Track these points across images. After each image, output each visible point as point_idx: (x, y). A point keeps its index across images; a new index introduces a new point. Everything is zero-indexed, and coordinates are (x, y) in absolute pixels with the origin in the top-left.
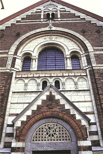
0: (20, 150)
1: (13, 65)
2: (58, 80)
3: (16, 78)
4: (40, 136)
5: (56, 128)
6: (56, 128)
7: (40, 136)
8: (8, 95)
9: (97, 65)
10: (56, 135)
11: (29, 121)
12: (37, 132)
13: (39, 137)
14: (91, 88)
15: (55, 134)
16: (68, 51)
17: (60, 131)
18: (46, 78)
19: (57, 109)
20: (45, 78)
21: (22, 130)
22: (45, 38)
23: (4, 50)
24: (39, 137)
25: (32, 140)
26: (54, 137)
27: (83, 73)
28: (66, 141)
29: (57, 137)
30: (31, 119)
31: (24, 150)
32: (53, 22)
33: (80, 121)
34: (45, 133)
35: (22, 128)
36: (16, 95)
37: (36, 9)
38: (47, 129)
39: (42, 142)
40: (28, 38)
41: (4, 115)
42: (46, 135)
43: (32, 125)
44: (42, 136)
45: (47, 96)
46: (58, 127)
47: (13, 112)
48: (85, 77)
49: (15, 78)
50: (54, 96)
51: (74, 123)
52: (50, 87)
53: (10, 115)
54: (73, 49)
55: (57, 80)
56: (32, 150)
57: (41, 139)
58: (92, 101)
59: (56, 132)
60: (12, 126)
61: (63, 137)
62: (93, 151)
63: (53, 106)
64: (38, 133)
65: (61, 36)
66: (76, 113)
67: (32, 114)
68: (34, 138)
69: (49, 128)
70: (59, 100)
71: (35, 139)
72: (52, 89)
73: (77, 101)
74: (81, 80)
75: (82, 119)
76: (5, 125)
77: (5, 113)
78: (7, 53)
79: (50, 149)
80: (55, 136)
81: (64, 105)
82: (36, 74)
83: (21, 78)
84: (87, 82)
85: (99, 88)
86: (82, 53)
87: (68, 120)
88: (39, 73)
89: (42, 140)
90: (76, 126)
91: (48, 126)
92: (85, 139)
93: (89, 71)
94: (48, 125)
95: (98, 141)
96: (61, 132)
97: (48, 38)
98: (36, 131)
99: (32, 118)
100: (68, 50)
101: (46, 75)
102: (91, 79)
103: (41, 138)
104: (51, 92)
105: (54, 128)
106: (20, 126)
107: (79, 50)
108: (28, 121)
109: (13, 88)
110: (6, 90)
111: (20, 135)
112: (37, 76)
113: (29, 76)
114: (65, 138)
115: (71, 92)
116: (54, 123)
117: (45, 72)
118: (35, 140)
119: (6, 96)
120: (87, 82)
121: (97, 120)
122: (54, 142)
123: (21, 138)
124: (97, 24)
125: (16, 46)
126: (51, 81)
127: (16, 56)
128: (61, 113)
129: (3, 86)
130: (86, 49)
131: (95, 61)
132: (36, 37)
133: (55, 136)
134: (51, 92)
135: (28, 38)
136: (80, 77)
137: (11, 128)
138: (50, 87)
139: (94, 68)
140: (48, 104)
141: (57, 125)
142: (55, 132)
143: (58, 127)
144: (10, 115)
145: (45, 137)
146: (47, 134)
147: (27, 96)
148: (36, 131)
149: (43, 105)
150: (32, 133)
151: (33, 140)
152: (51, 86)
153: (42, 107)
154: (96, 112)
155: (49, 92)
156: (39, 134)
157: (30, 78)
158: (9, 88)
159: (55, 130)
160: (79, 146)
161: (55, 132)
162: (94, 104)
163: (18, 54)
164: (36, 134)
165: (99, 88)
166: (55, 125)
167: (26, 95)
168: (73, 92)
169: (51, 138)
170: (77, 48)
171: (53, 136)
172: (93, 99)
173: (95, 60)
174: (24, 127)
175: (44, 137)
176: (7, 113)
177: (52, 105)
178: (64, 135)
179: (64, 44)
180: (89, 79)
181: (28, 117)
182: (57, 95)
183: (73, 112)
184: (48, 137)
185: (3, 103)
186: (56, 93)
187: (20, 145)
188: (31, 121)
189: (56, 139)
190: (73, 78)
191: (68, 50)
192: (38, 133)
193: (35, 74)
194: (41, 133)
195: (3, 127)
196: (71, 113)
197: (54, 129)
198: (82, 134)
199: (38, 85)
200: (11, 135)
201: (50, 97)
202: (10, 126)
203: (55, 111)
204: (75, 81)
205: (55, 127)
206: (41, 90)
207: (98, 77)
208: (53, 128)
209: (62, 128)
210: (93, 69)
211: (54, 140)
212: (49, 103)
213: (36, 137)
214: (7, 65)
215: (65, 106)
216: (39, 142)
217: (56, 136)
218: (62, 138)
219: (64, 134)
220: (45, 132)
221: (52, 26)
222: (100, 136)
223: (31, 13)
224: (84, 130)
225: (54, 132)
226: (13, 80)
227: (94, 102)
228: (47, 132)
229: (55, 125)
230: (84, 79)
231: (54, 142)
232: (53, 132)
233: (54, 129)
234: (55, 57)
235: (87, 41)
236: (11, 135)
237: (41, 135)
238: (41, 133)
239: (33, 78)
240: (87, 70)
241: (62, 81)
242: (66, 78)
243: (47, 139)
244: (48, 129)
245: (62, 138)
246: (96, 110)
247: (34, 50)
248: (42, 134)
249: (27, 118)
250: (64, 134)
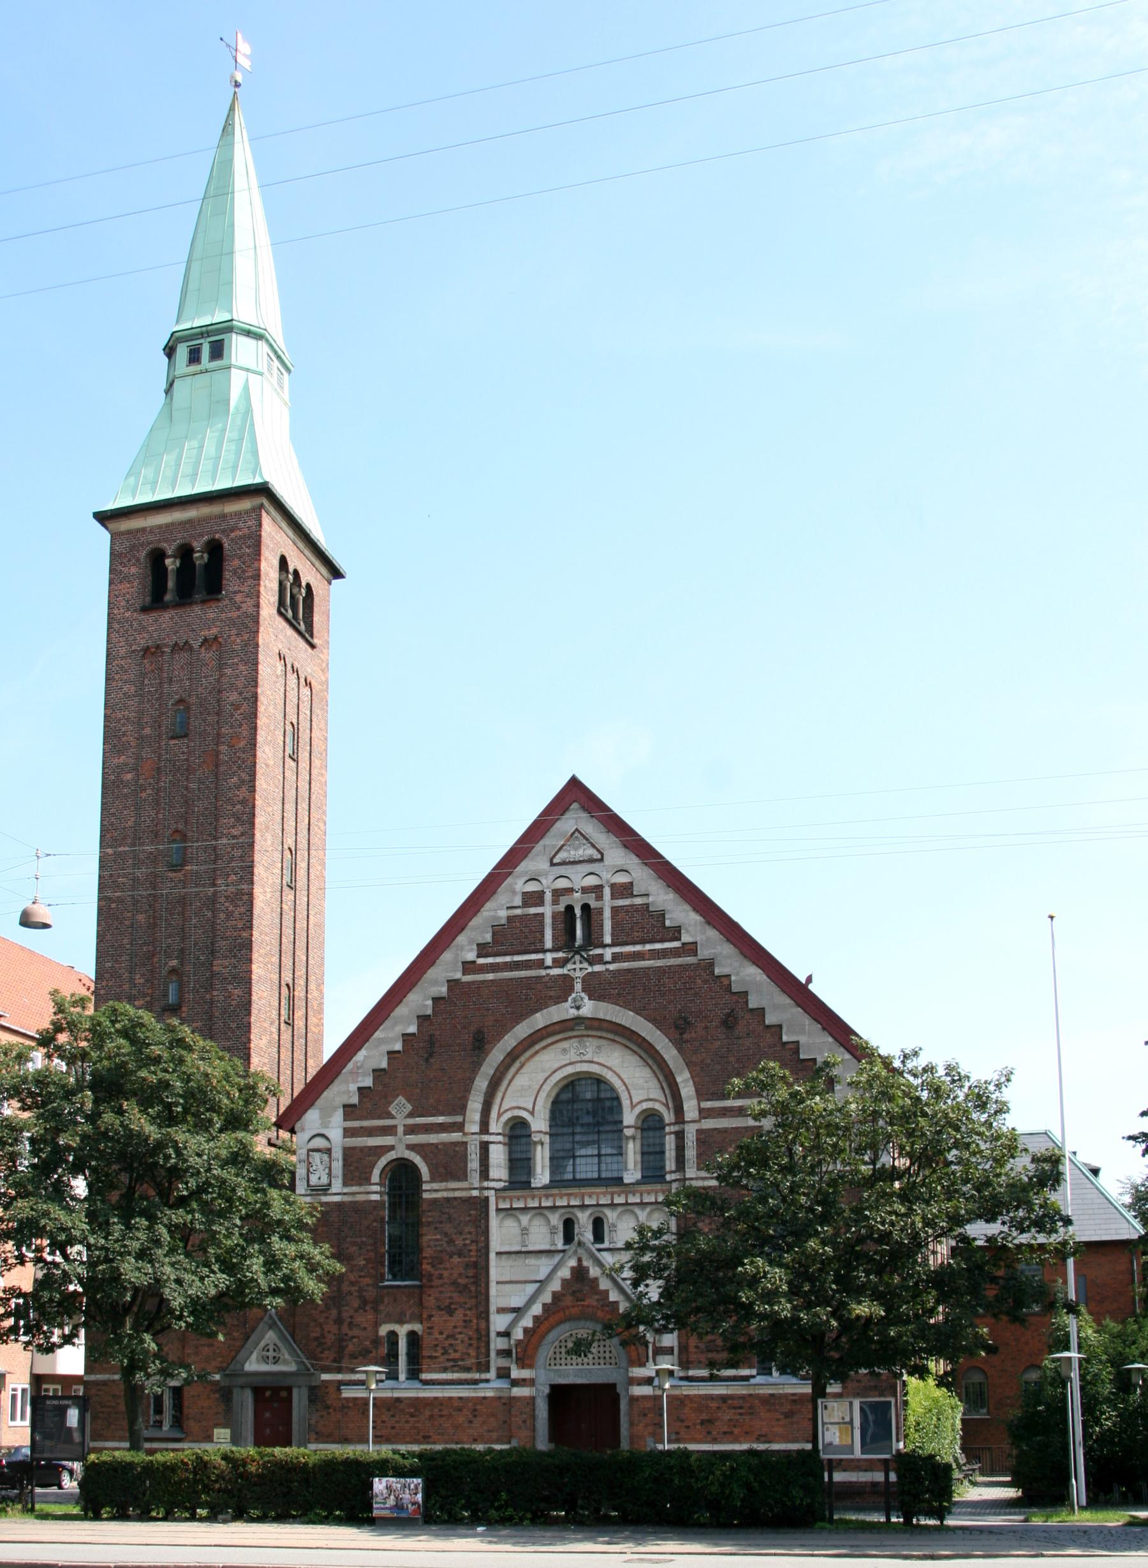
1: (485, 1174)
3: (498, 1210)
9: (699, 1172)
11: (538, 1327)
21: (527, 1345)
22: (564, 1051)
23: (449, 1114)
32: (586, 972)
36: (506, 1262)
37: (526, 878)
40: (513, 1056)
43: (543, 1337)
45: (573, 1268)
50: (587, 1270)
53: (501, 1310)
55: (598, 1215)
60: (506, 1334)
64: (558, 1350)
65: (614, 1041)
71: (553, 1362)
76: (493, 1335)
78: (460, 1127)
79: (579, 1381)
81: (606, 1292)
82: (547, 1196)
83: (510, 1211)
86: (668, 1117)
104: (580, 1260)
109: (495, 1245)
111: (524, 1356)
118: (552, 1364)
122: (588, 1367)
124: (733, 978)
125: (481, 1099)
126: (584, 1220)
127: (486, 1138)
130: (679, 1110)
132: (537, 1047)
134: (580, 1260)
135: (513, 1056)
137: (505, 1339)
144: (501, 1310)
150: (545, 1353)
157: (533, 1212)
163: (493, 1128)
174: (529, 1340)
176: (493, 1308)
178: (607, 1355)
181: (536, 1319)
186: (591, 1261)
187: (526, 1374)
188: (543, 1328)
189: (591, 1363)
192: (558, 1350)
193: (543, 1199)
199: (553, 1232)
203: (588, 1306)
216: (561, 1367)
218: (602, 1361)
219: (607, 1353)
223: (508, 908)
226: (494, 1220)
241: (611, 1221)
242: (620, 1209)
249: (534, 1322)
250: (607, 1353)
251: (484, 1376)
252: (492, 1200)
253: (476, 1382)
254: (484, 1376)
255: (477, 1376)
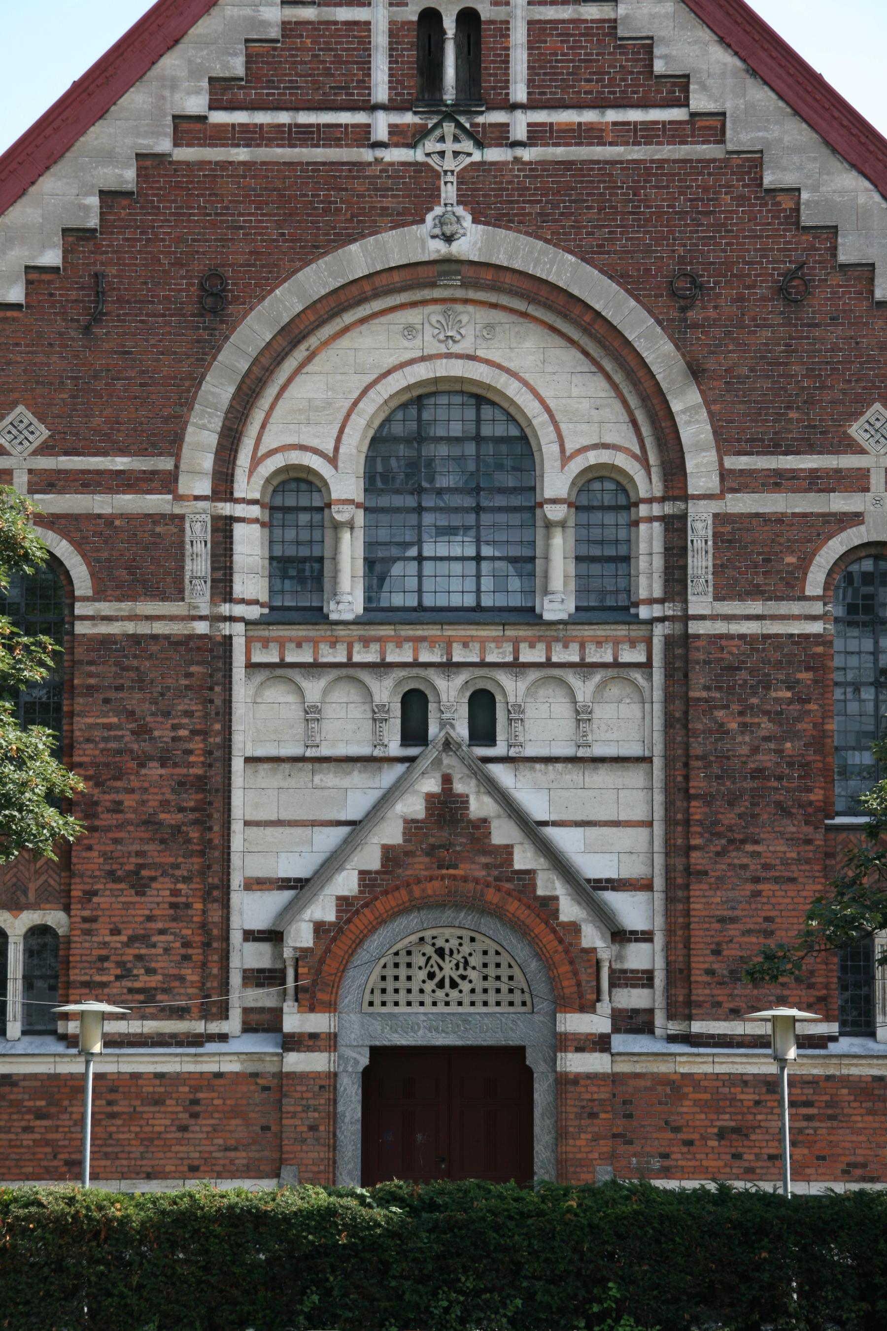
0: (318, 1043)
2: (490, 687)
3: (251, 666)
4: (398, 985)
5: (470, 955)
6: (470, 955)
7: (398, 985)
8: (230, 785)
9: (717, 605)
10: (470, 981)
11: (349, 921)
12: (385, 966)
13: (396, 991)
14: (658, 750)
15: (463, 977)
16: (563, 466)
17: (485, 965)
18: (422, 672)
19: (477, 866)
20: (415, 671)
21: (322, 961)
24: (396, 991)
25: (365, 1004)
26: (461, 991)
27: (633, 644)
28: (511, 1009)
29: (473, 991)
30: (357, 912)
31: (335, 1042)
32: (468, 160)
33: (574, 928)
34: (422, 975)
35: (319, 953)
36: (265, 776)
38: (429, 958)
39: (409, 1010)
41: (225, 888)
42: (424, 982)
44: (408, 985)
45: (430, 798)
46: (479, 947)
47: (258, 867)
48: (638, 676)
49: (246, 667)
50: (463, 801)
51: (549, 939)
52: (444, 750)
53: (255, 884)
54: (595, 447)
55: (481, 685)
56: (369, 1043)
57: (402, 997)
58: (650, 824)
59: (469, 969)
61: (498, 991)
62: (612, 1055)
63: (458, 852)
64: (390, 972)
66: (560, 889)
67: (360, 892)
68: (372, 992)
69: (440, 952)
70: (485, 821)
71: (377, 1000)
72: (454, 758)
73: (579, 817)
74: (615, 690)
75: (585, 920)
76: (236, 937)
77: (229, 880)
79: (440, 1040)
80: (465, 986)
81: (508, 850)
82: (366, 642)
84: (647, 706)
85: (697, 758)
87: (524, 924)
88: (379, 639)
89: (409, 1004)
90: (556, 951)
91: (434, 945)
92: (588, 1007)
93: (669, 643)
94: (434, 938)
95: (651, 1011)
96: (491, 971)
97: (429, 331)
98: (383, 961)
99: (363, 907)
100: (563, 449)
101: (424, 657)
102: (668, 698)
103: (403, 993)
104: (447, 780)
105: (459, 952)
106: (310, 944)
107: (634, 456)
108: (346, 923)
110: (210, 753)
112: (371, 656)
113: (328, 655)
114: (505, 997)
115: (550, 767)
116: (460, 932)
117: (419, 633)
119: (217, 790)
120: (647, 706)
121: (659, 922)
123: (320, 995)
125: (217, 423)
128: (491, 890)
129: (194, 732)
131: (710, 577)
133: (465, 986)
134: (447, 780)
136: (611, 672)
137: (265, 948)
138: (444, 750)
139: (695, 628)
140: (432, 840)
141: (473, 940)
142: (465, 969)
143: (479, 947)
144: (255, 884)
145: (422, 991)
146: (431, 976)
147: (323, 785)
148: (383, 961)
149: (411, 847)
151: (371, 1004)
152: (448, 745)
153: (407, 854)
154: (659, 883)
155: (438, 775)
156: (396, 978)
157: (334, 673)
158: (224, 740)
159: (466, 963)
160: (561, 1034)
161: (465, 969)
162: (658, 845)
163: (241, 489)
164: (384, 978)
165: (697, 758)
166: (466, 941)
167: (317, 779)
168: (559, 766)
169: (447, 995)
170: (622, 435)
171: (454, 985)
172: (659, 813)
173: (711, 569)
174: (328, 950)
175: (415, 989)
177: (455, 845)
179: (542, 402)
180: (658, 695)
182: (479, 792)
183: (547, 887)
184: (434, 991)
185: (210, 829)
186: (473, 782)
188: (359, 923)
189: (466, 1000)
190: (571, 678)
191: (563, 449)
192: (390, 972)
194: (403, 972)
195: (228, 945)
196: (540, 892)
197: (461, 955)
198: (579, 984)
199: (378, 717)
200: (266, 978)
201: (444, 803)
202: (256, 940)
203: (465, 879)
204: (580, 698)
205: (466, 949)
206: (395, 748)
207: (707, 688)
208: (455, 952)
209: (497, 953)
210: (686, 636)
211: (460, 1004)
212: (438, 836)
213: (384, 991)
214: (187, 581)
215: (511, 853)
216: (396, 1010)
217: (470, 986)
218: (492, 997)
220: (420, 968)
221: (460, 210)
222: (657, 993)
224: (589, 971)
225: (461, 971)
227: (658, 829)
228: (428, 968)
229: (466, 941)
230: (629, 690)
231: (460, 1009)
232: (457, 968)
233: (461, 955)
234: (478, 505)
235: (694, 397)
236: (266, 978)
237: (402, 984)
238: (403, 972)
239: (351, 671)
240: (659, 630)
241: (511, 699)
242: (533, 675)
243: (428, 1000)
244: (435, 957)
245: (492, 997)
246: (663, 872)
247: (336, 449)
248: (409, 978)
251: (215, 1027)
252: (239, 644)
253: (197, 1040)
254: (215, 1027)
255: (199, 1027)
